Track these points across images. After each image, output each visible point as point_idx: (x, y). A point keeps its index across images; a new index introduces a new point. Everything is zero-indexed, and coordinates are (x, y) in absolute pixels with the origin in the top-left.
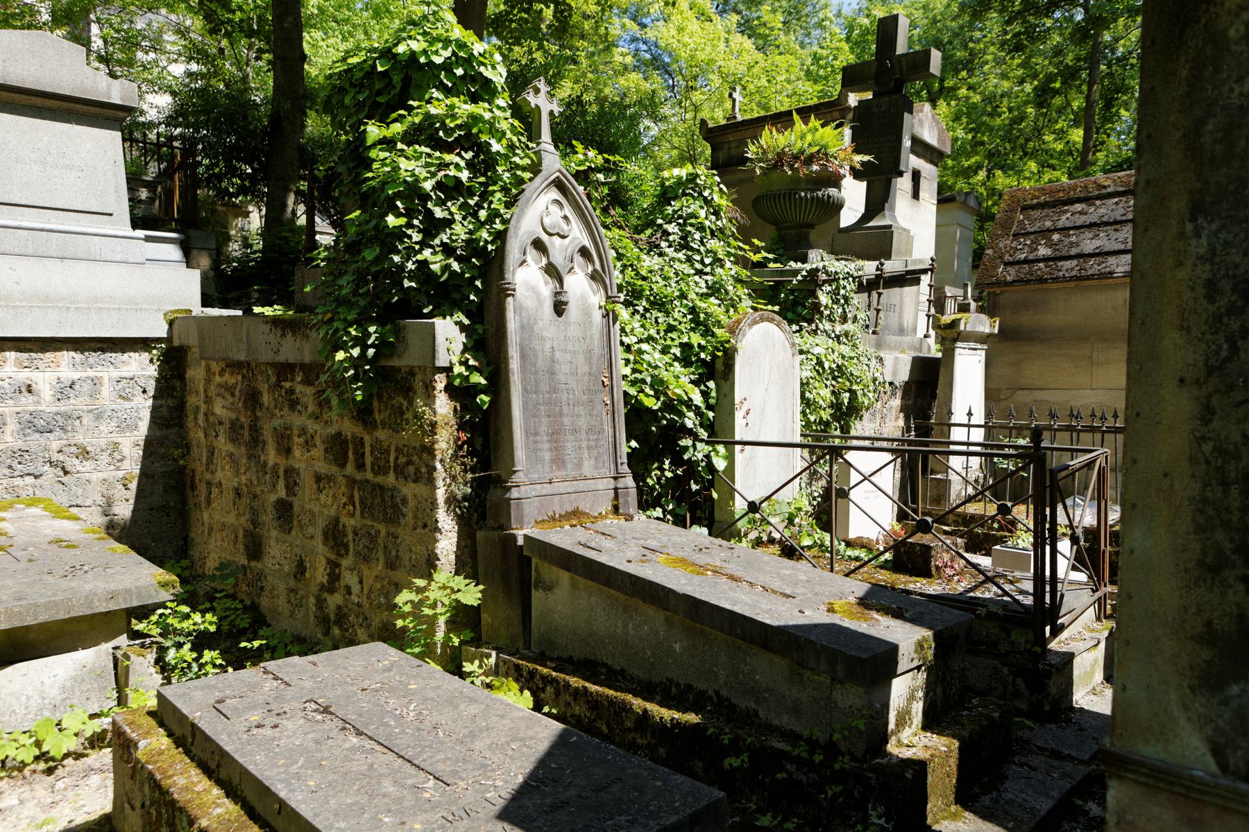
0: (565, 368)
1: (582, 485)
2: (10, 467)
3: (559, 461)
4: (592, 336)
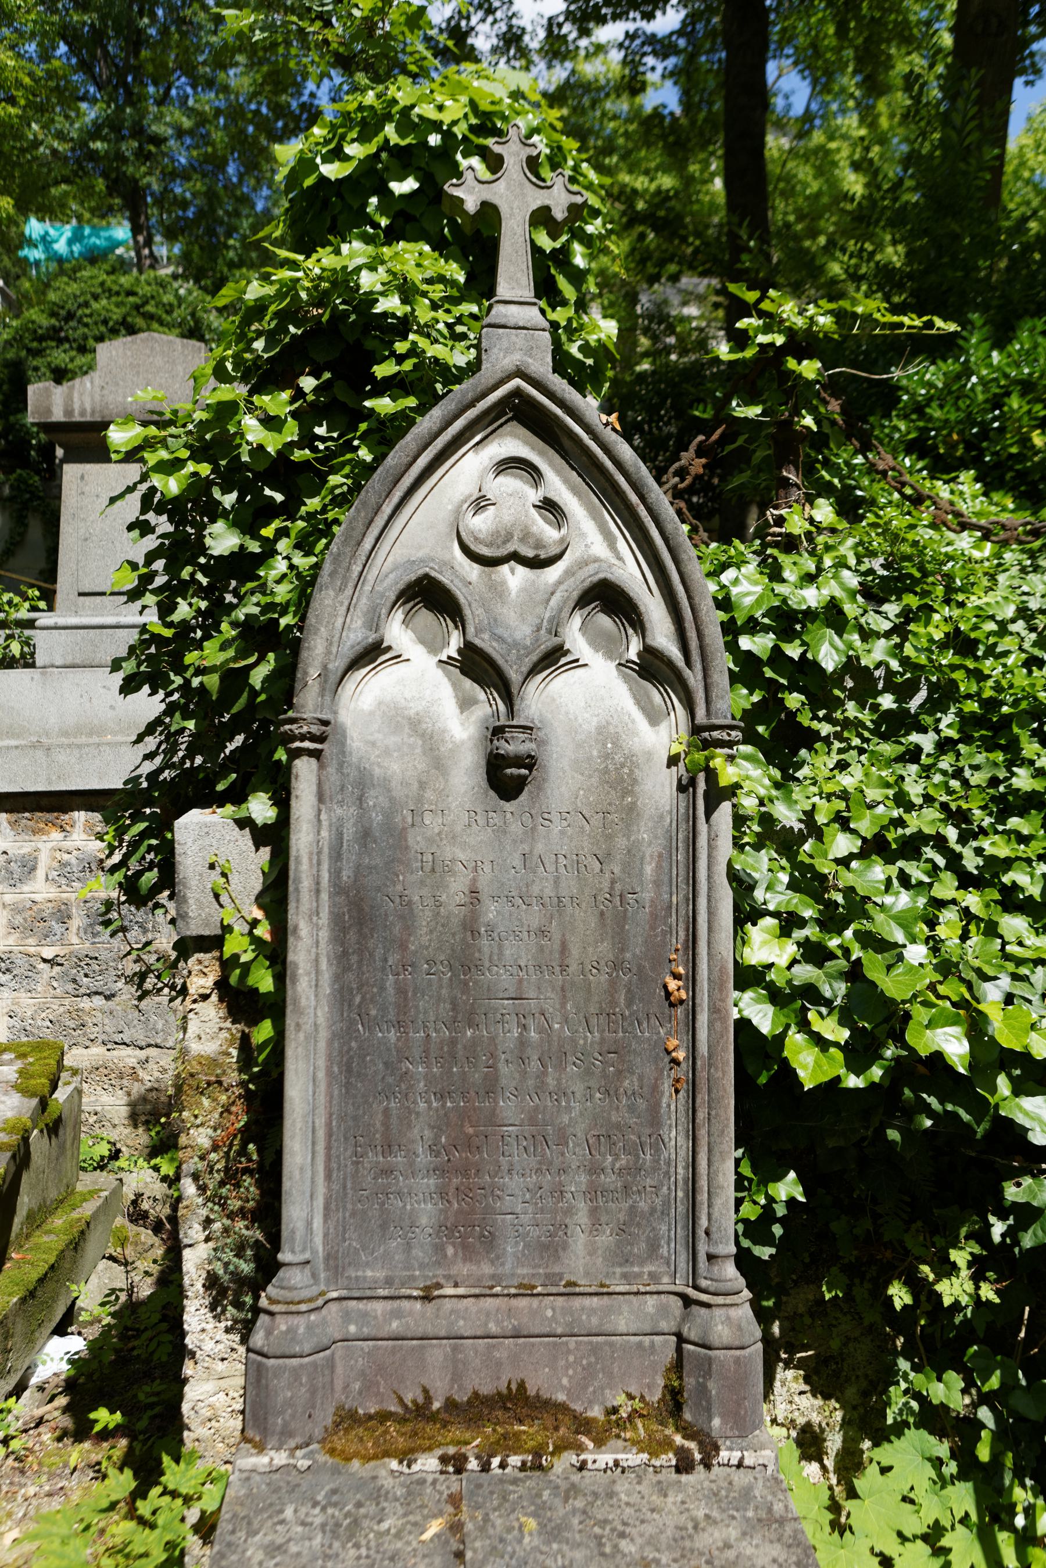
0: (519, 951)
1: (550, 1311)
2: (74, 981)
3: (470, 1229)
4: (632, 852)
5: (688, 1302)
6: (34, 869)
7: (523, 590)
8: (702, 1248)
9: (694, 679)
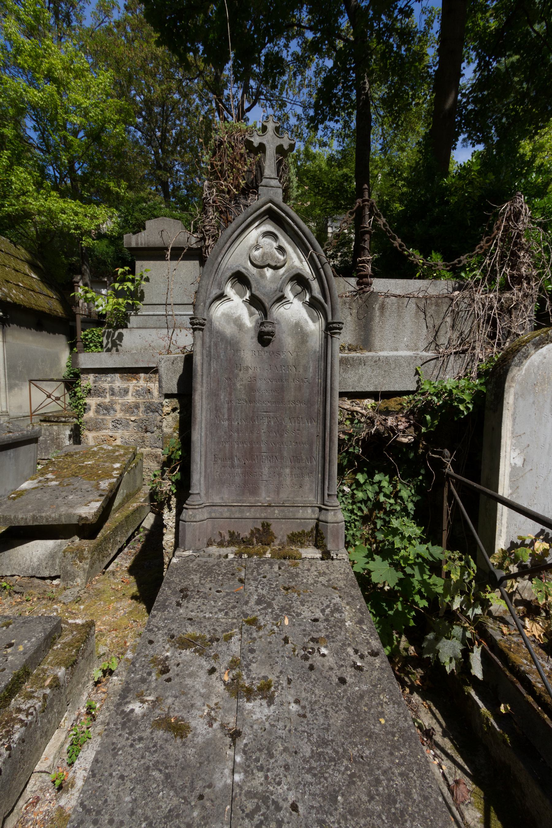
5: (321, 509)
6: (128, 392)
7: (271, 277)
8: (326, 492)
9: (328, 307)
